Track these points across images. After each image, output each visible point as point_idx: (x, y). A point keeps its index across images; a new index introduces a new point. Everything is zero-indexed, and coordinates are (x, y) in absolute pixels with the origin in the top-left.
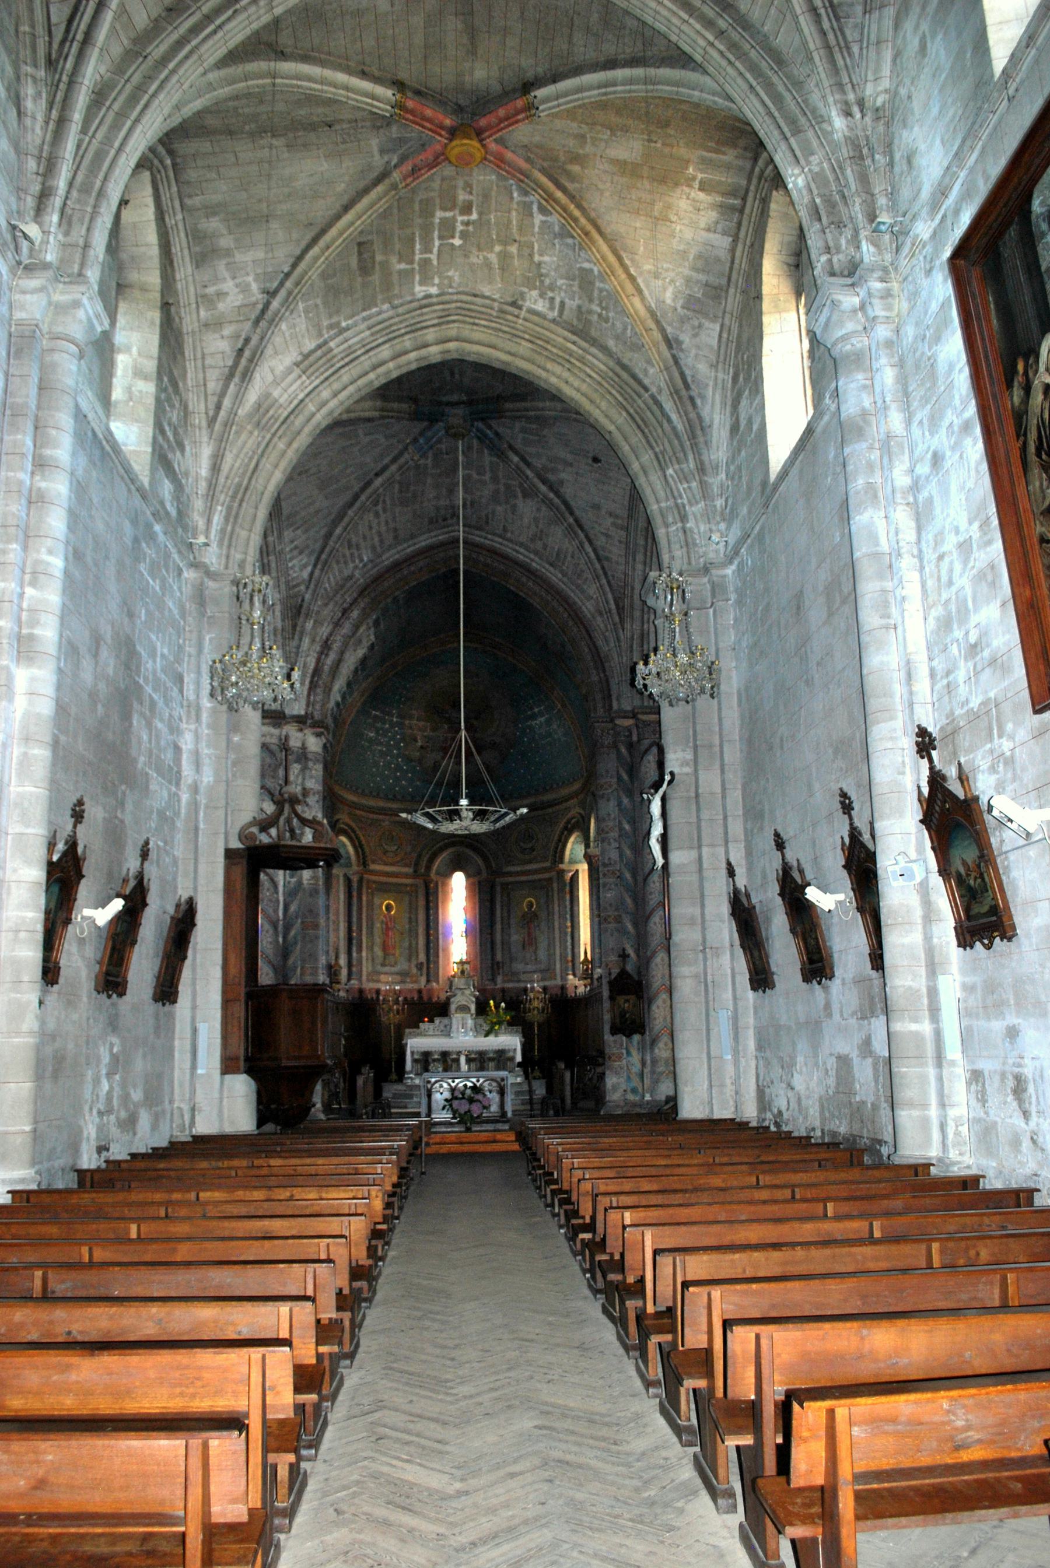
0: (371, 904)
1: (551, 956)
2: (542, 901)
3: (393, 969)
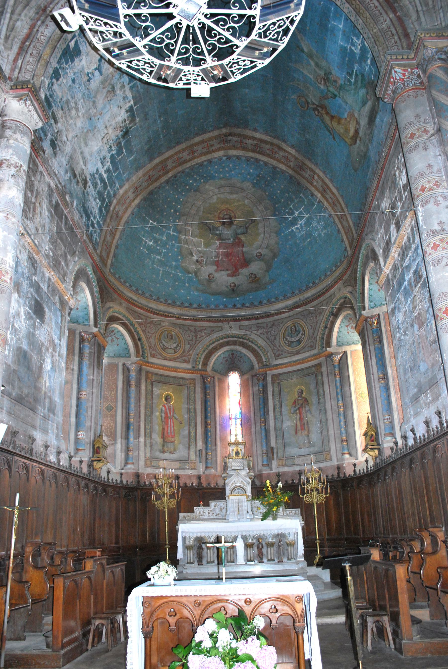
0: (149, 394)
1: (325, 439)
2: (312, 387)
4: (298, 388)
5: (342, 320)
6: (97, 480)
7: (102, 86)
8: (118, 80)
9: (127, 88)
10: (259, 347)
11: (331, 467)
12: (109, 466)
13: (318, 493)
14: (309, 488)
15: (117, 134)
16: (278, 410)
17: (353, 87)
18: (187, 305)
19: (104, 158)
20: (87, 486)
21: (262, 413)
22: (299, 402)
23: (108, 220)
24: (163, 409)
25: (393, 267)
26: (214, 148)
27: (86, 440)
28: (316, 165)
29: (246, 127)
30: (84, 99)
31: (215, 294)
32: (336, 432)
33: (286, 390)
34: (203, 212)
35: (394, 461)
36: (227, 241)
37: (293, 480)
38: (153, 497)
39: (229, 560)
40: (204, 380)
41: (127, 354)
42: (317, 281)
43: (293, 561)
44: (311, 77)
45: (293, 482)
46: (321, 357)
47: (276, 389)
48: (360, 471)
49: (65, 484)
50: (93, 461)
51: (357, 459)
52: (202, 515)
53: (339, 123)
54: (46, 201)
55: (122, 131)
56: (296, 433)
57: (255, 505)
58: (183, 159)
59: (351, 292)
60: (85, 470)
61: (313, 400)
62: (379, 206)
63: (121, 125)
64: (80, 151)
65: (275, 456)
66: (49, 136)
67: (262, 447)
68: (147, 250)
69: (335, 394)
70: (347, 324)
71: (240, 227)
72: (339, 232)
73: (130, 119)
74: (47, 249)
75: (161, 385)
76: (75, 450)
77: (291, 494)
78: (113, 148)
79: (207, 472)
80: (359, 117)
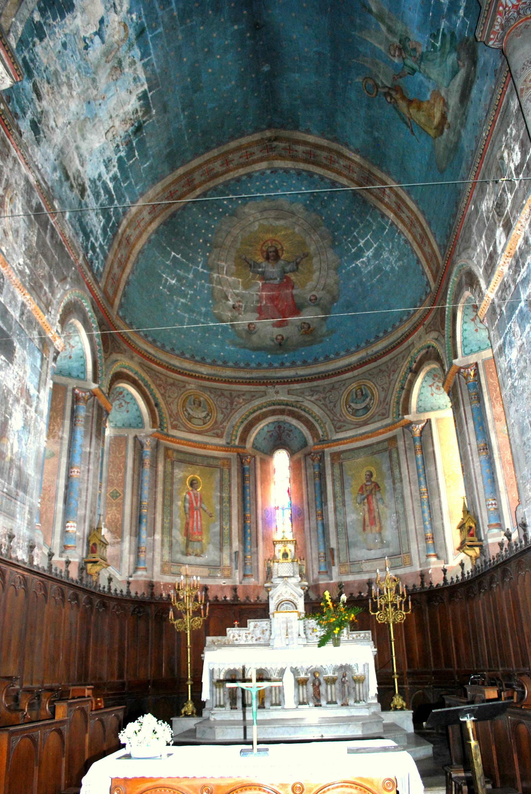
0: (169, 478)
2: (385, 467)
3: (199, 560)
4: (365, 470)
5: (424, 378)
6: (92, 589)
7: (104, 59)
8: (126, 52)
9: (139, 66)
10: (314, 417)
11: (412, 574)
12: (111, 570)
13: (396, 609)
14: (383, 603)
15: (125, 129)
16: (339, 499)
17: (439, 53)
18: (220, 363)
19: (110, 160)
20: (76, 597)
21: (318, 503)
22: (368, 488)
23: (116, 246)
24: (188, 497)
25: (500, 287)
26: (255, 157)
27: (78, 534)
28: (388, 173)
29: (296, 128)
30: (79, 73)
31: (256, 349)
32: (417, 527)
33: (350, 473)
34: (242, 243)
35: (482, 574)
36: (272, 282)
37: (360, 593)
38: (171, 613)
39: (274, 702)
40: (241, 458)
41: (140, 424)
42: (390, 330)
43: (363, 703)
44: (382, 48)
45: (360, 596)
46: (395, 428)
47: (337, 471)
48: (452, 579)
49: (40, 593)
50: (86, 563)
51: (447, 563)
52: (237, 640)
53: (419, 109)
54: (21, 198)
55: (133, 125)
56: (364, 529)
57: (310, 626)
58: (215, 171)
59: (436, 339)
60: (74, 574)
61: (386, 485)
62: (477, 210)
63: (132, 117)
64: (75, 144)
65: (336, 560)
66: (29, 115)
67: (319, 548)
68: (168, 291)
69: (416, 476)
70: (431, 384)
71: (289, 263)
72: (418, 262)
73: (143, 109)
74: (22, 263)
75: (183, 465)
76: (61, 547)
77: (359, 610)
78: (121, 148)
79: (246, 582)
80: (447, 94)
